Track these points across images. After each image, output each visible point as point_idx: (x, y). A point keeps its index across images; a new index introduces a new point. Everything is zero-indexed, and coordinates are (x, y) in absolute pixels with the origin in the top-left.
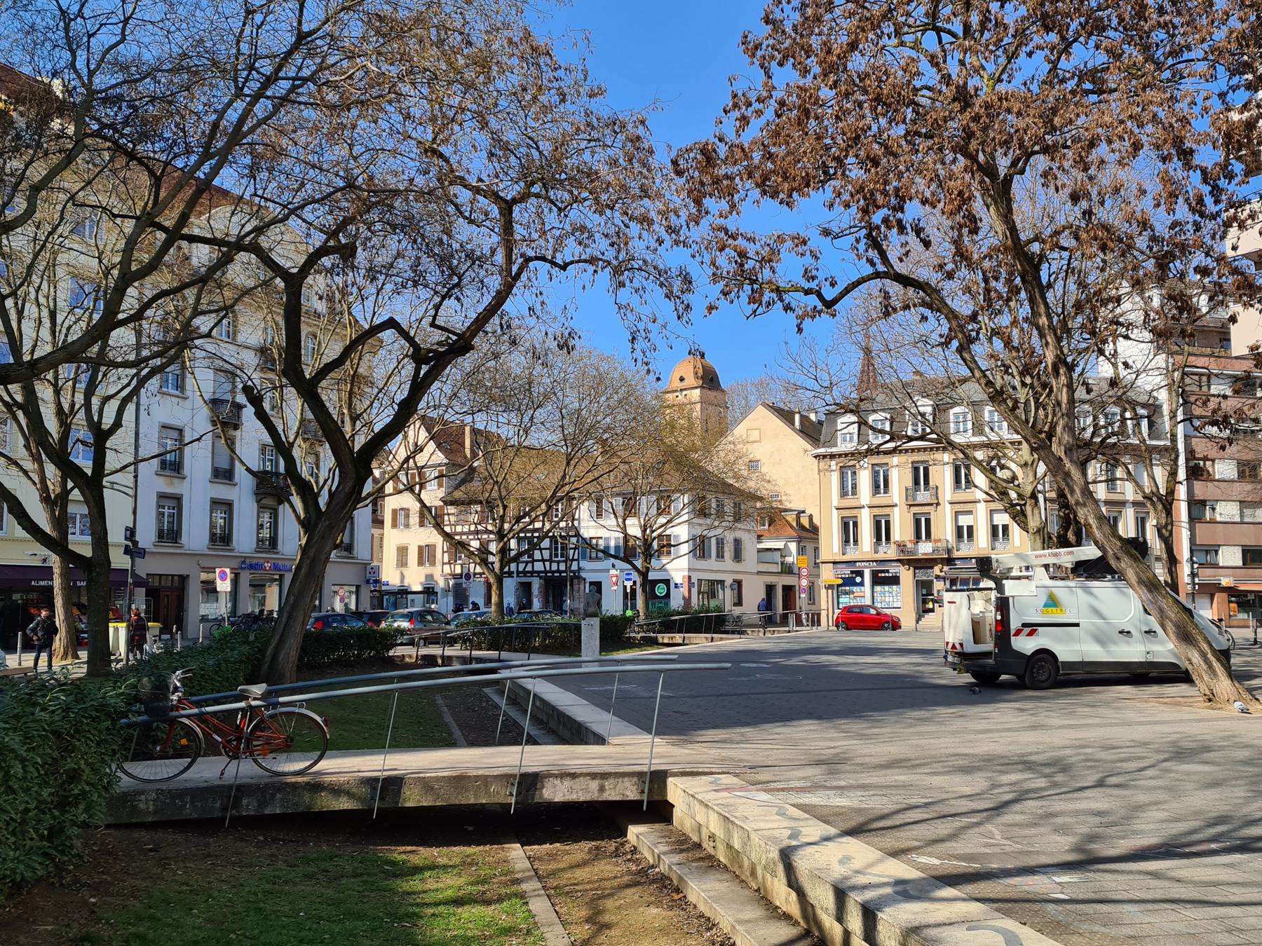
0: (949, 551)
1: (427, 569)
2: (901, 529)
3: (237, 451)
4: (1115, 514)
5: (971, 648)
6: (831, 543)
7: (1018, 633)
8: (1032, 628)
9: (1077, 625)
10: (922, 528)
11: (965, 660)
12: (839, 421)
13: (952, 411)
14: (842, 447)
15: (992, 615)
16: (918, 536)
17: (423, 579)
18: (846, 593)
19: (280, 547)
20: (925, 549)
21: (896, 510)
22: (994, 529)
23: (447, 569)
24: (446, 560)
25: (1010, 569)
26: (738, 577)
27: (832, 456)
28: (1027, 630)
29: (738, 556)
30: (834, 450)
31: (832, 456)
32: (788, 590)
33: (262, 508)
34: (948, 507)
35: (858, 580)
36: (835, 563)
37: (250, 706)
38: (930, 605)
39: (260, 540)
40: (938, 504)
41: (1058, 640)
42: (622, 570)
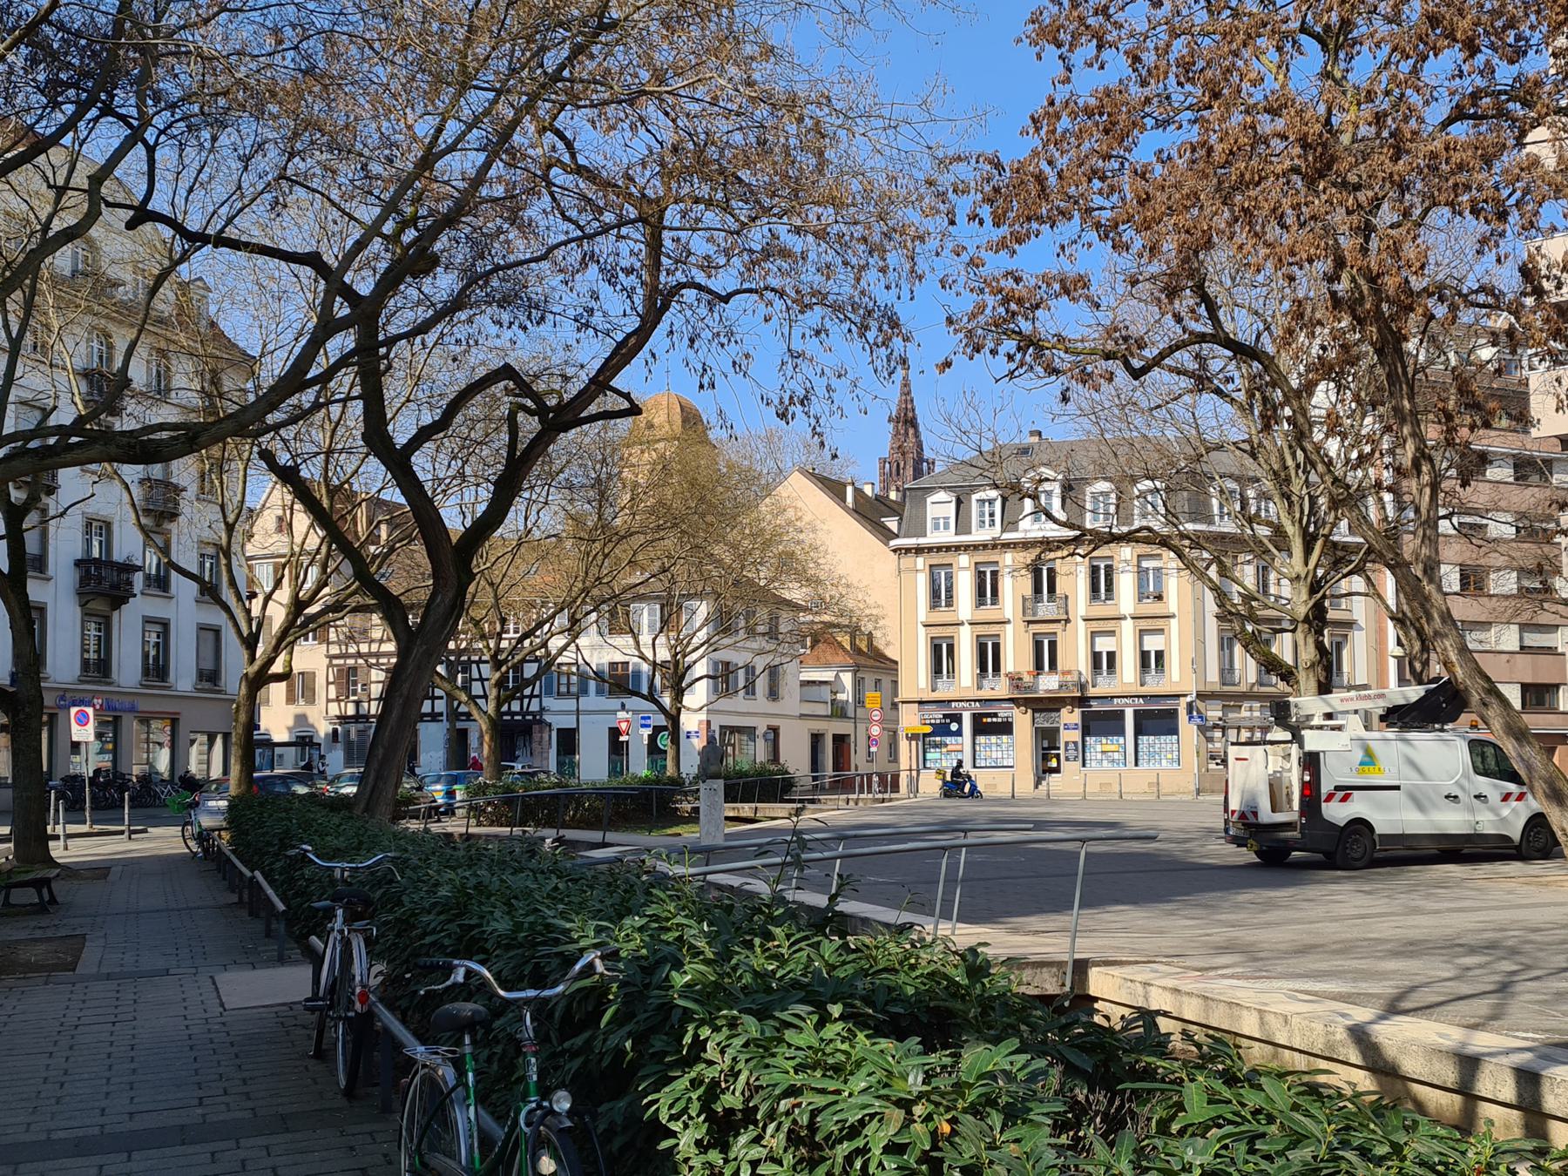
0: (1083, 687)
1: (301, 707)
2: (1017, 656)
3: (1209, 596)
4: (1339, 639)
5: (1266, 815)
6: (915, 678)
7: (1330, 797)
8: (1345, 792)
9: (1397, 788)
10: (1045, 654)
11: (1248, 828)
12: (929, 500)
13: (1089, 490)
14: (932, 538)
15: (1294, 777)
16: (1039, 666)
17: (291, 723)
18: (936, 746)
19: (114, 675)
20: (1048, 684)
21: (1009, 628)
22: (1144, 656)
23: (334, 709)
24: (333, 695)
25: (1309, 717)
26: (774, 722)
27: (919, 550)
28: (1341, 794)
29: (773, 694)
30: (922, 541)
31: (919, 550)
32: (840, 741)
33: (87, 614)
34: (1081, 625)
35: (954, 727)
36: (920, 703)
37: (391, 911)
38: (1054, 763)
39: (85, 664)
40: (1067, 621)
41: (1380, 806)
42: (635, 712)
